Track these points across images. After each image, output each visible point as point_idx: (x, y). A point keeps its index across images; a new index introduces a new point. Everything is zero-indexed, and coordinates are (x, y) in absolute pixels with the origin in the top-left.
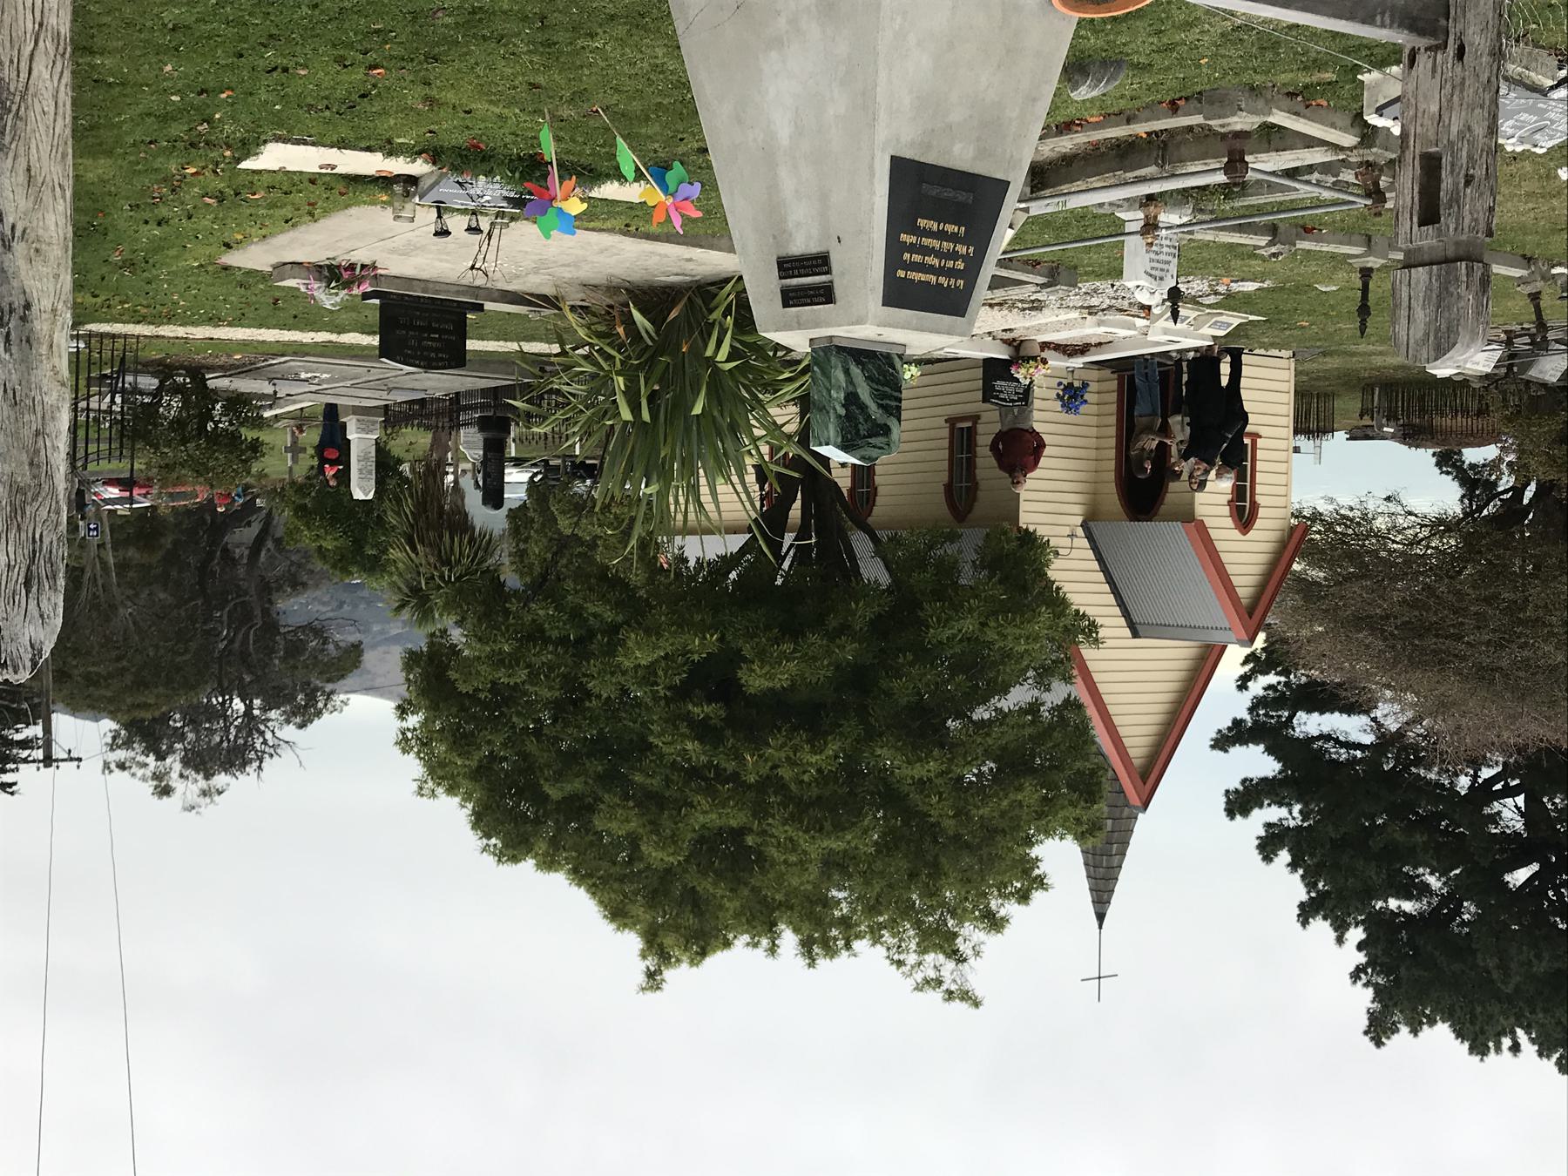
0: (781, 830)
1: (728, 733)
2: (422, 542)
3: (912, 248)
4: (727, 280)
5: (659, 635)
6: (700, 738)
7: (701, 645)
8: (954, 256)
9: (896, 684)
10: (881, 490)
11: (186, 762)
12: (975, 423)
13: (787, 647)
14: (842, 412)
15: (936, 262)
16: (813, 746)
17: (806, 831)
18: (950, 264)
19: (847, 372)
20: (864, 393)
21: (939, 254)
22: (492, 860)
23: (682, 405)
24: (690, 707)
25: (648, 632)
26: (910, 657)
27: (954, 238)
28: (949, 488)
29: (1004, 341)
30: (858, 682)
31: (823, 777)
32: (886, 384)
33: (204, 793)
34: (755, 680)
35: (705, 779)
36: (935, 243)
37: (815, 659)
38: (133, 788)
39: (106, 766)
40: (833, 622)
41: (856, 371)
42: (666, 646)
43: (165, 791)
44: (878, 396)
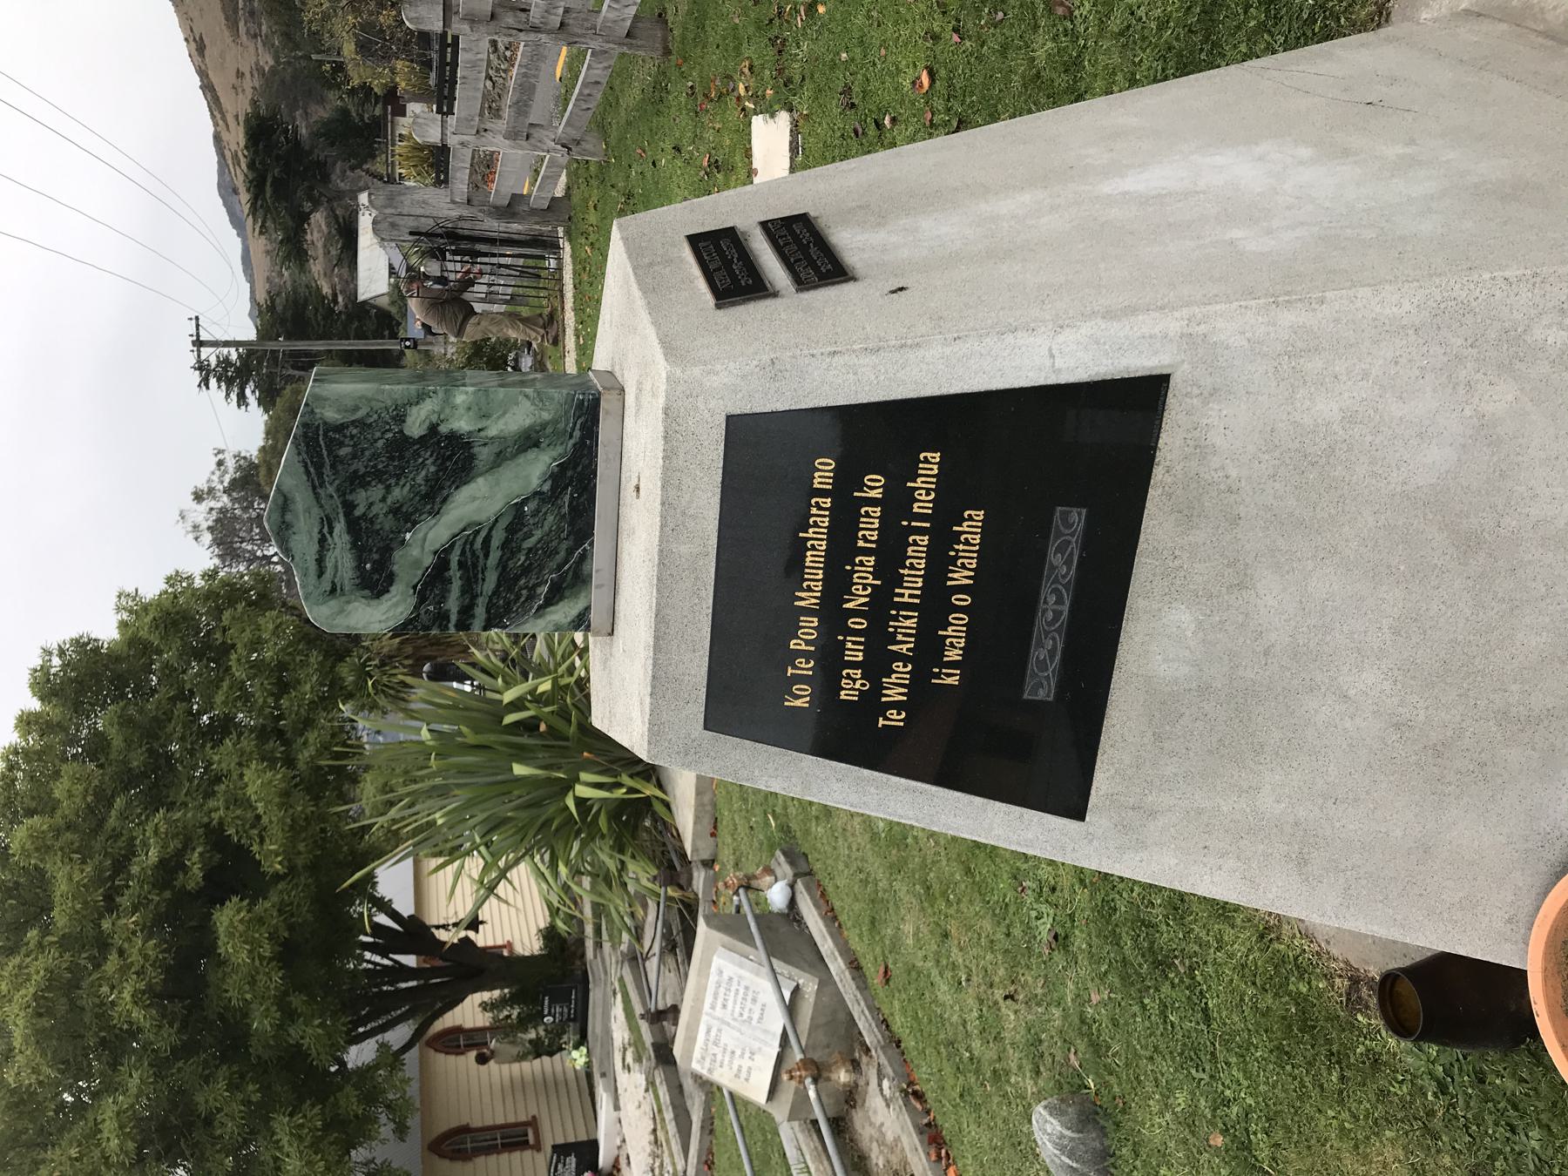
0: (39, 967)
1: (167, 894)
2: (401, 643)
3: (897, 503)
4: (660, 786)
5: (281, 806)
6: (162, 863)
7: (271, 855)
8: (877, 667)
9: (222, 1084)
10: (462, 1058)
11: (222, 511)
12: (532, 1147)
13: (267, 950)
14: (415, 425)
15: (858, 599)
16: (143, 992)
17: (35, 997)
18: (855, 652)
19: (529, 440)
20: (477, 502)
21: (882, 605)
22: (37, 662)
23: (522, 754)
24: (199, 849)
25: (286, 794)
26: (256, 1097)
27: (929, 649)
28: (465, 1129)
29: (617, 1160)
30: (230, 1039)
31: (103, 1010)
32: (507, 580)
33: (196, 527)
34: (228, 917)
35: (112, 878)
36: (911, 589)
37: (253, 982)
38: (202, 473)
39: (220, 452)
40: (297, 1001)
41: (535, 470)
42: (272, 816)
43: (198, 497)
44: (467, 553)
